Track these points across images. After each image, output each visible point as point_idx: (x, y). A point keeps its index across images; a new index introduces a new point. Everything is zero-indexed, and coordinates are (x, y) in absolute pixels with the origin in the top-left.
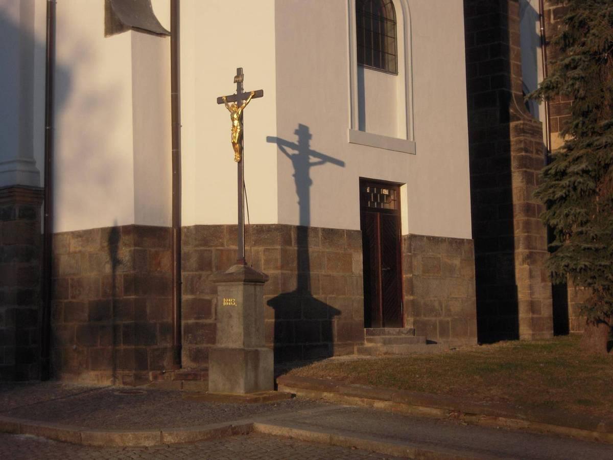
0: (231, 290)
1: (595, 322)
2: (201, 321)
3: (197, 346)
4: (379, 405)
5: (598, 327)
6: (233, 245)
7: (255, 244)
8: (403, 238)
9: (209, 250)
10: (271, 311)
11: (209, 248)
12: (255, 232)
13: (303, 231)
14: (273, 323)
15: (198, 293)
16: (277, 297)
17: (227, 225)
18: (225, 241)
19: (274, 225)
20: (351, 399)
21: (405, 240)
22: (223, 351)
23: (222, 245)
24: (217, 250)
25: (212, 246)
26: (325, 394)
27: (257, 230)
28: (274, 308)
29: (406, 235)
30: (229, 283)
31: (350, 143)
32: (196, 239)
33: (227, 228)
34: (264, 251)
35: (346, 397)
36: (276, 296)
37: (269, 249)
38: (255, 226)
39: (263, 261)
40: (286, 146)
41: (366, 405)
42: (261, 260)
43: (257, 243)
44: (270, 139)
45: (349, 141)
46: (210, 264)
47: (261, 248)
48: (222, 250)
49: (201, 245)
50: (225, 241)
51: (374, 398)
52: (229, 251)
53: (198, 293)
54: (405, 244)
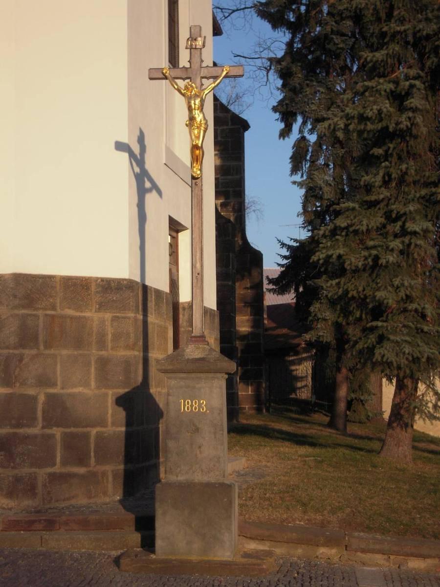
0: (198, 386)
1: (403, 425)
2: (21, 431)
3: (16, 471)
4: (415, 564)
5: (406, 432)
6: (69, 308)
7: (99, 309)
8: (181, 306)
9: (34, 315)
10: (122, 414)
11: (35, 312)
12: (100, 289)
13: (145, 288)
14: (123, 435)
15: (18, 385)
16: (128, 393)
17: (61, 276)
18: (58, 301)
19: (125, 280)
20: (367, 557)
21: (184, 309)
22: (187, 488)
23: (54, 308)
24: (46, 315)
25: (37, 309)
26: (322, 550)
27: (103, 287)
28: (125, 409)
29: (186, 303)
30: (193, 375)
31: (165, 164)
32: (15, 296)
33: (60, 281)
34: (112, 320)
35: (359, 554)
36: (127, 390)
37: (118, 317)
38: (99, 280)
39: (110, 336)
40: (135, 161)
41: (393, 564)
42: (107, 334)
43: (102, 307)
44: (120, 146)
45: (164, 162)
46: (35, 338)
47: (108, 316)
48: (53, 316)
49: (24, 307)
50: (58, 301)
51: (408, 555)
52: (64, 317)
53: (18, 385)
54: (184, 315)
